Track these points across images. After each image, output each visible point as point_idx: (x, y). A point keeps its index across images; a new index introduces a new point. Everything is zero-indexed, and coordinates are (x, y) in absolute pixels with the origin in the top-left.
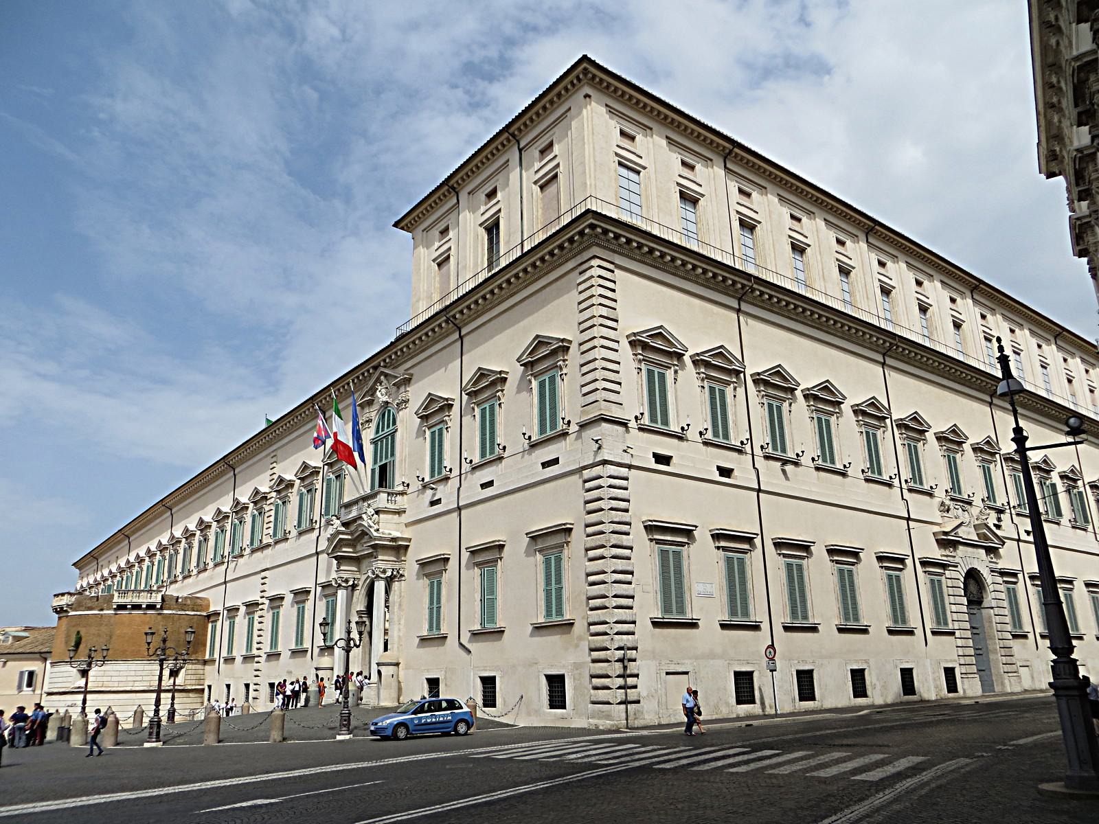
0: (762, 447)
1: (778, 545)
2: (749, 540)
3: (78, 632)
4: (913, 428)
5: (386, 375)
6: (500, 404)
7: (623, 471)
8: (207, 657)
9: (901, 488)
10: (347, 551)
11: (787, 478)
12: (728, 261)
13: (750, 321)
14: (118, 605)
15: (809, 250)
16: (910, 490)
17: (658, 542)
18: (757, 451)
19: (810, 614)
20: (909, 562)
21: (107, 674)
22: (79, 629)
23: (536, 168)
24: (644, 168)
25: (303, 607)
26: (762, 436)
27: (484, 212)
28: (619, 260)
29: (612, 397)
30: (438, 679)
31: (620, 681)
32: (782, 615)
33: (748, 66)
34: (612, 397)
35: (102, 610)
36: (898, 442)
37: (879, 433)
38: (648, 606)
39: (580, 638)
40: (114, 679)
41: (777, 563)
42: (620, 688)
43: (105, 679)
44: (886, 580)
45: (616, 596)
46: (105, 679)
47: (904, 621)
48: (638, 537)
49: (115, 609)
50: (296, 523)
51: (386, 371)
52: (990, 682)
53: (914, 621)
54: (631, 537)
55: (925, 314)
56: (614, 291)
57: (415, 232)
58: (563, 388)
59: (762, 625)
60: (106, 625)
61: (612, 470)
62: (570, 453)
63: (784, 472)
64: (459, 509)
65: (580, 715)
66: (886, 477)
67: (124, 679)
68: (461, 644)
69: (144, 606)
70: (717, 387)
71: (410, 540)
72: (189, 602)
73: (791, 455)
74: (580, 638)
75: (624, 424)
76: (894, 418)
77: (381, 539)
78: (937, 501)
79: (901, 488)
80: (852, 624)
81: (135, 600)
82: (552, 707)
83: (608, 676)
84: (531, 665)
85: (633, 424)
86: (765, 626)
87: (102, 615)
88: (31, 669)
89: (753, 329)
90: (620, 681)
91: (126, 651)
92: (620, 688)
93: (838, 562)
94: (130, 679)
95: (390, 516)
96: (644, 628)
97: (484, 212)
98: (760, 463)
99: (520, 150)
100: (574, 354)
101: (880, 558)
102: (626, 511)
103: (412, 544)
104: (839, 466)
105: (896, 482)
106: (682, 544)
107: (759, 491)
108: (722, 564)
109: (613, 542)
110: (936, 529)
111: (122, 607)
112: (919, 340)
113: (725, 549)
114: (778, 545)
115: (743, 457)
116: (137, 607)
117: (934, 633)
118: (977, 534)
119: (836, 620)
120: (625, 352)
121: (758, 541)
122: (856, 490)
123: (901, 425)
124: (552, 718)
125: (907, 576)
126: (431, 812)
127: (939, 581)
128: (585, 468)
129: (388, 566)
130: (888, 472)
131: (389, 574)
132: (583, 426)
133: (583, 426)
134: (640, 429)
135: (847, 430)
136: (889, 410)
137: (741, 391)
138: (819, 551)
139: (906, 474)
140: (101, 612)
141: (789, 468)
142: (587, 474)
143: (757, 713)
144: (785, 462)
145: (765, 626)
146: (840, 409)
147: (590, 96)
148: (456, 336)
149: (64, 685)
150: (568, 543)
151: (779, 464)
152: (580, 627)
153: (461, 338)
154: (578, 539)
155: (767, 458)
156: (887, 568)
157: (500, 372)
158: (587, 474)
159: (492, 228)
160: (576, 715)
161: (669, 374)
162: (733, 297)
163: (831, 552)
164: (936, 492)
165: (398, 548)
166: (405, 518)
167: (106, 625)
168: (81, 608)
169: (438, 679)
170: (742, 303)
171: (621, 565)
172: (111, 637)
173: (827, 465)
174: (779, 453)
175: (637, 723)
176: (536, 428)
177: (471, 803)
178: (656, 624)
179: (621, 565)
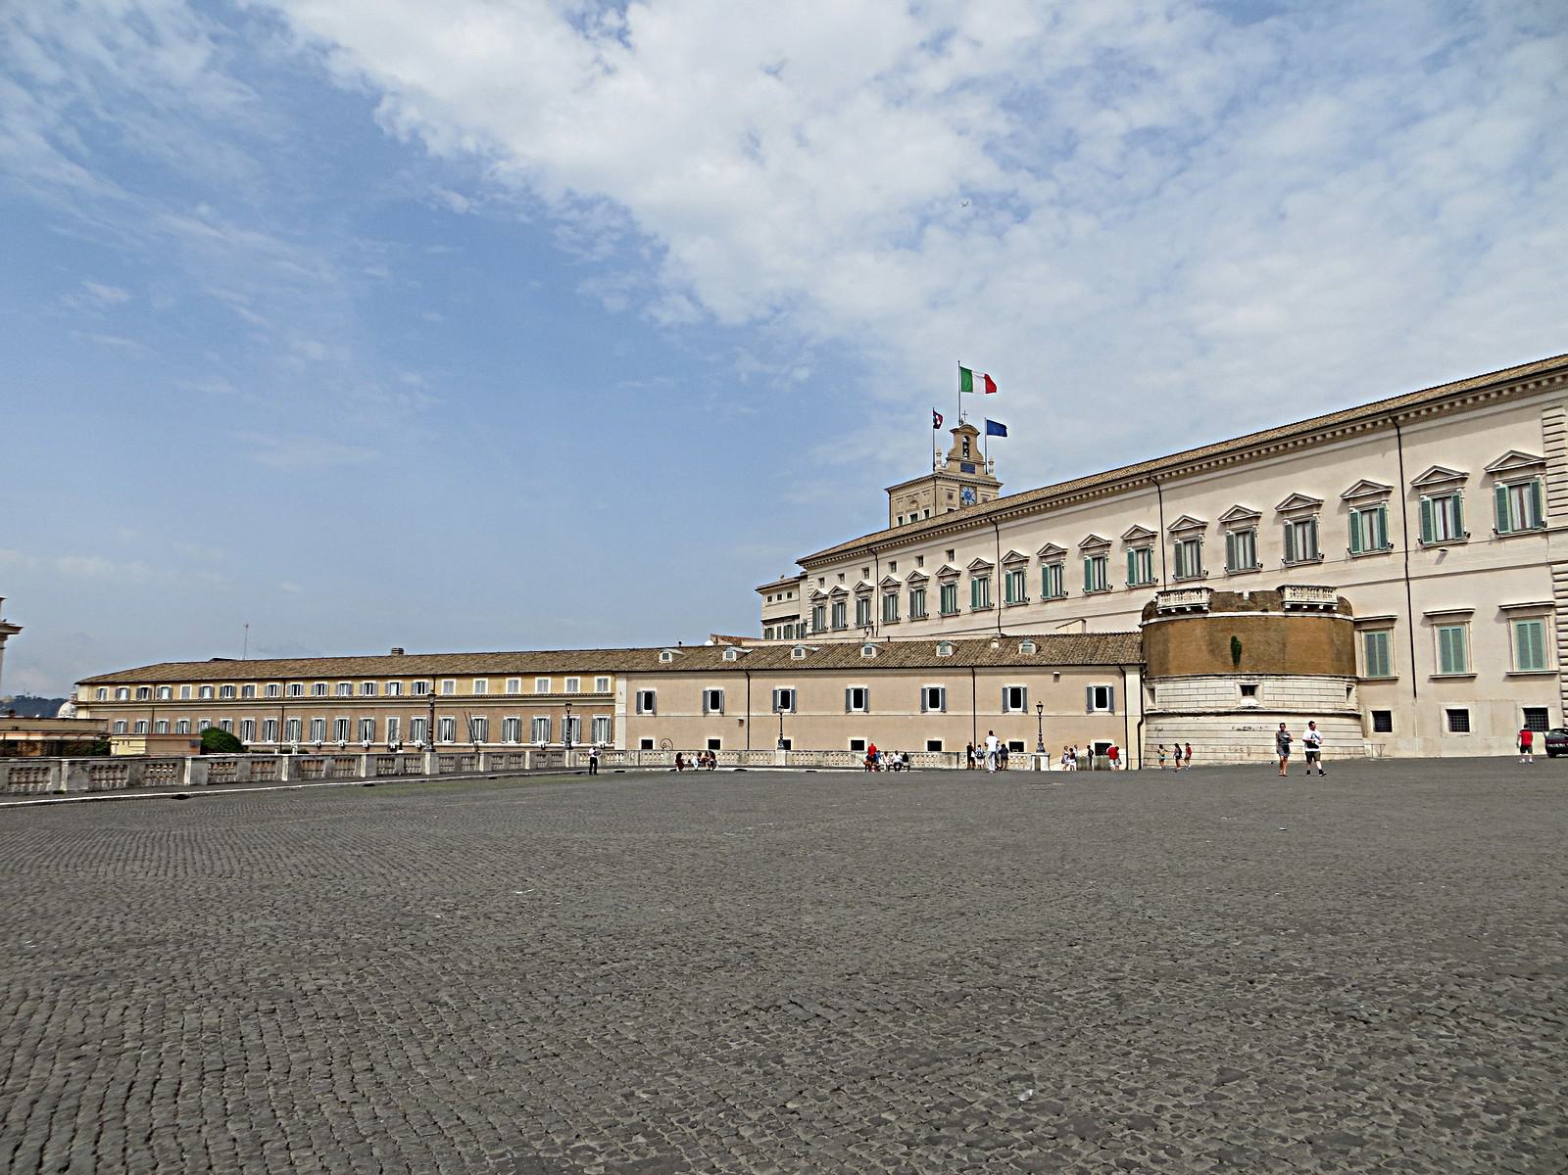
3: (1234, 639)
8: (1362, 672)
14: (1292, 605)
21: (1287, 691)
22: (1235, 635)
33: (962, 187)
35: (1266, 610)
40: (1297, 698)
43: (1286, 698)
46: (1286, 698)
52: (55, 745)
60: (1275, 630)
67: (1309, 698)
69: (1321, 607)
81: (1312, 599)
87: (1267, 617)
88: (1101, 684)
91: (1304, 664)
94: (1315, 698)
111: (1296, 607)
116: (1313, 608)
140: (1265, 614)
143: (1256, 759)
149: (1219, 704)
150: (1392, 628)
153: (1399, 436)
167: (1275, 630)
168: (1229, 608)
169: (1390, 712)
172: (1284, 645)
178: (1435, 679)
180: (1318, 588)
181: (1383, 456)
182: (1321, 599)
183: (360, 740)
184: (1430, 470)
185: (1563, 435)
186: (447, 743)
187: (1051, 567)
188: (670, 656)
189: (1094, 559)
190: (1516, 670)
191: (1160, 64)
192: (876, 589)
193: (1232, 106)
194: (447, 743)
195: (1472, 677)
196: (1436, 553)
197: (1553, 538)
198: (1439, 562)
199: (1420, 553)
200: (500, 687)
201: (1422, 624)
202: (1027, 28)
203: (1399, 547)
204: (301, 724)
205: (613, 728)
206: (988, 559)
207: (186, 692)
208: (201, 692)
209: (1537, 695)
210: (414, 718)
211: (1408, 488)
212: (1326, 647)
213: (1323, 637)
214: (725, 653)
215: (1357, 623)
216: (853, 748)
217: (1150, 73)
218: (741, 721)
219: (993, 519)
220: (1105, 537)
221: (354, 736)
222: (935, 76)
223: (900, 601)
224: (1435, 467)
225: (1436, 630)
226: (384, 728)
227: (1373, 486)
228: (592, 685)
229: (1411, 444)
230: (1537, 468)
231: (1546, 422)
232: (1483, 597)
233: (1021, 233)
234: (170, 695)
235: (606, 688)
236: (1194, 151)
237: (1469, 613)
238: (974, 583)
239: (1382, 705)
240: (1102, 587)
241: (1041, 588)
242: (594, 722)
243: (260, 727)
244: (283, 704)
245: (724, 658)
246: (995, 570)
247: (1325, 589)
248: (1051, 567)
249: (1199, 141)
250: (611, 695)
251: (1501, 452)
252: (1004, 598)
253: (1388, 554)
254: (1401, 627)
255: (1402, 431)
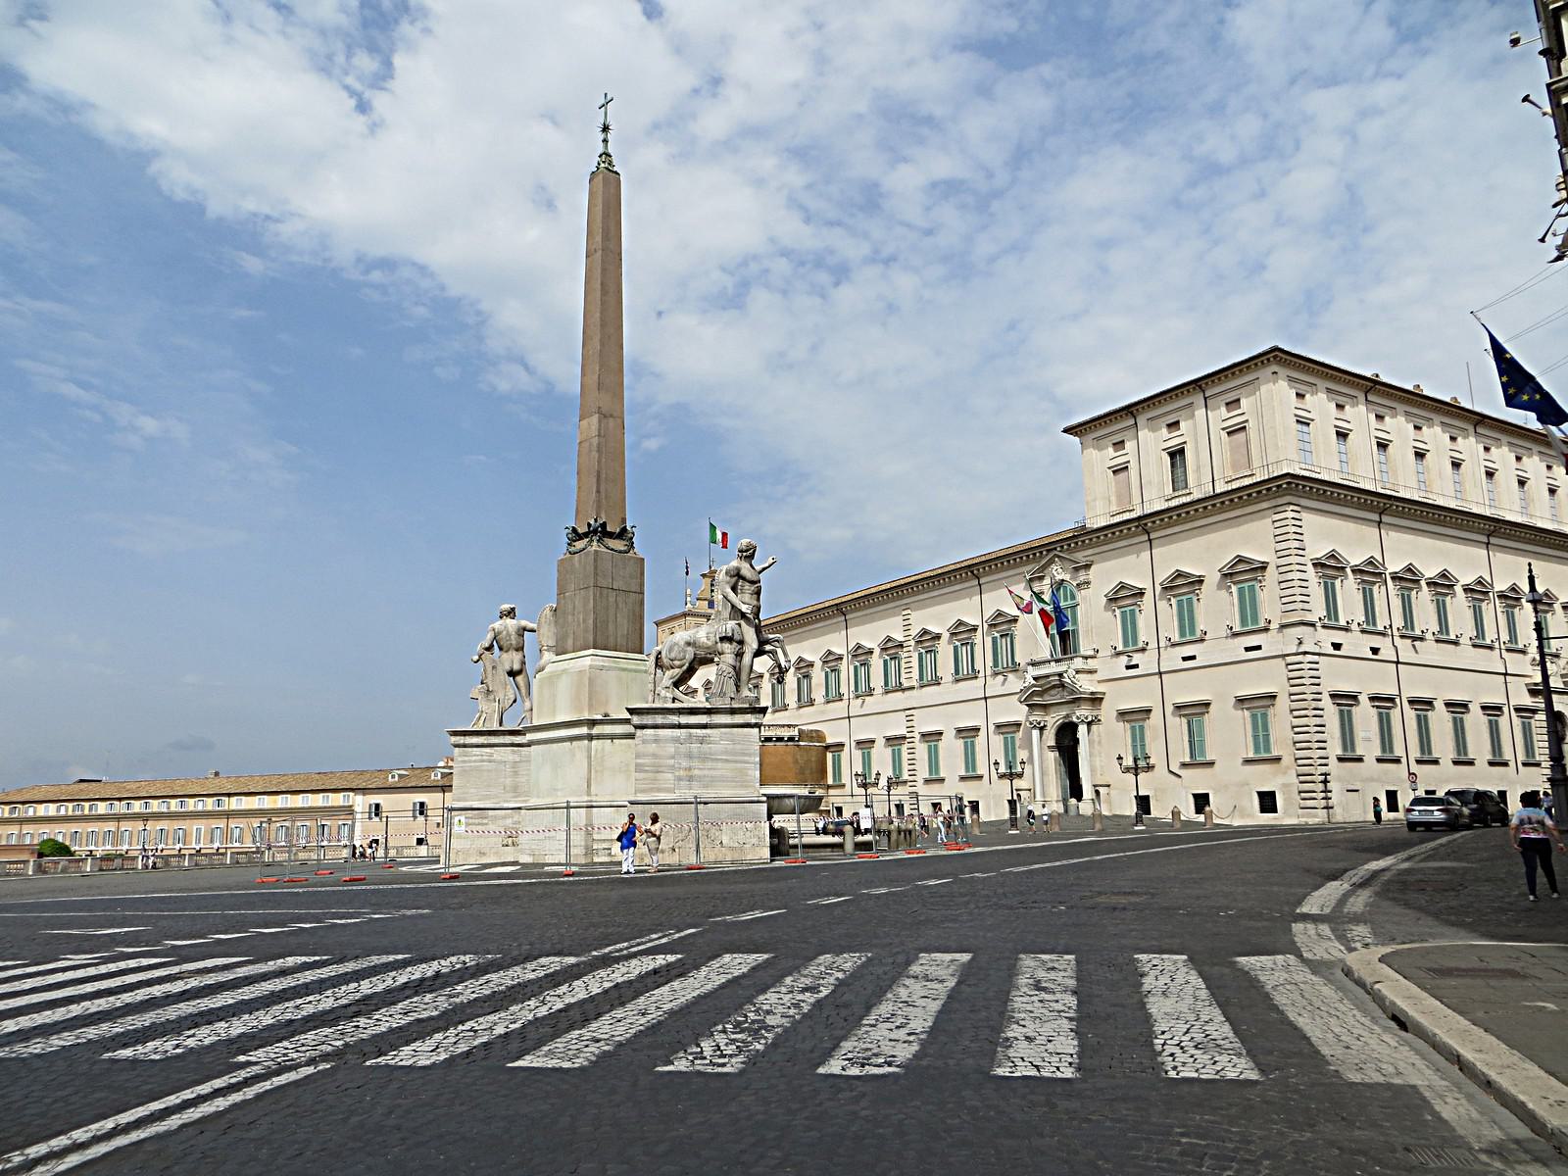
0: (1398, 629)
1: (1411, 702)
2: (1392, 700)
4: (1408, 579)
5: (1059, 557)
6: (1198, 600)
7: (1316, 658)
8: (830, 781)
9: (1500, 649)
10: (1037, 700)
11: (1417, 652)
12: (1372, 488)
13: (1392, 534)
15: (1428, 455)
16: (1508, 650)
17: (1338, 705)
18: (1395, 632)
19: (1433, 751)
20: (1506, 709)
23: (1220, 415)
24: (1313, 420)
25: (973, 743)
26: (1398, 622)
27: (1167, 439)
28: (1304, 502)
29: (1306, 606)
30: (1148, 796)
31: (1323, 795)
32: (1415, 753)
34: (1306, 606)
36: (1499, 610)
37: (1484, 605)
38: (1335, 749)
39: (1288, 768)
41: (1411, 714)
42: (1323, 799)
44: (1487, 724)
45: (1317, 742)
47: (1500, 755)
48: (1326, 702)
49: (762, 741)
50: (953, 671)
51: (1061, 554)
53: (1508, 755)
54: (1323, 702)
55: (1523, 487)
56: (1301, 527)
57: (1085, 438)
58: (1263, 597)
59: (1402, 760)
61: (1309, 658)
62: (1269, 643)
63: (1414, 646)
64: (1160, 674)
65: (1290, 816)
66: (1488, 642)
68: (1171, 772)
70: (1368, 587)
71: (1104, 694)
72: (814, 735)
73: (1418, 632)
74: (1288, 768)
75: (1313, 625)
76: (1496, 590)
77: (1085, 693)
78: (1529, 657)
79: (1500, 649)
80: (1463, 758)
82: (1262, 811)
83: (1314, 792)
84: (1243, 785)
85: (1318, 624)
86: (1404, 760)
89: (1392, 537)
90: (1323, 795)
92: (1323, 799)
93: (1453, 712)
95: (1085, 675)
96: (1333, 761)
97: (1167, 439)
98: (1397, 640)
99: (1205, 399)
100: (1271, 570)
101: (1484, 708)
102: (1318, 685)
103: (1106, 697)
104: (1453, 637)
105: (1497, 645)
106: (1351, 705)
107: (1398, 663)
108: (1375, 719)
109: (1314, 706)
110: (1528, 680)
112: (1519, 519)
113: (1378, 707)
114: (1411, 702)
115: (1387, 638)
116: (780, 739)
117: (1524, 764)
118: (1564, 682)
119: (1452, 755)
120: (1311, 572)
121: (1398, 700)
122: (1467, 656)
123: (1502, 596)
124: (1267, 819)
125: (1503, 721)
126: (236, 1097)
127: (1529, 723)
128: (1288, 655)
129: (1086, 713)
130: (1490, 636)
131: (1090, 719)
132: (1283, 627)
133: (1283, 627)
134: (1323, 627)
135: (1459, 605)
136: (1492, 585)
137: (1383, 588)
138: (1439, 705)
139: (1505, 637)
141: (1417, 643)
142: (1290, 659)
144: (1415, 639)
145: (1404, 760)
146: (1454, 590)
147: (1276, 373)
148: (843, 618)
150: (1273, 705)
151: (1409, 641)
152: (1287, 760)
153: (846, 620)
154: (1283, 703)
155: (1402, 637)
156: (1489, 715)
157: (1200, 576)
158: (1290, 659)
159: (1177, 455)
160: (1286, 815)
161: (1338, 583)
162: (1375, 512)
163: (1448, 705)
164: (1529, 650)
165: (1096, 700)
166: (1096, 677)
169: (1148, 796)
170: (1383, 517)
171: (1318, 721)
173: (1444, 639)
174: (1410, 632)
175: (1333, 821)
176: (1238, 622)
177: (207, 1109)
179: (1318, 721)
180: (783, 726)
181: (1138, 556)
182: (786, 733)
183: (174, 844)
184: (1173, 574)
185: (910, 627)
186: (237, 845)
187: (1001, 636)
188: (397, 776)
189: (861, 665)
190: (1251, 755)
191: (939, 111)
192: (845, 658)
193: (1020, 156)
194: (237, 845)
195: (1211, 764)
196: (1000, 678)
197: (907, 693)
198: (1003, 683)
199: (1229, 640)
200: (275, 802)
201: (1173, 714)
202: (796, 71)
203: (982, 674)
204: (131, 833)
205: (353, 831)
206: (972, 620)
207: (47, 809)
208: (58, 810)
209: (1266, 779)
210: (214, 826)
211: (1158, 588)
212: (792, 765)
213: (790, 759)
214: (433, 774)
215: (827, 747)
216: (418, 844)
217: (929, 121)
218: (438, 824)
219: (975, 572)
220: (935, 630)
221: (170, 841)
222: (714, 122)
223: (814, 681)
224: (1239, 556)
225: (1128, 725)
226: (192, 834)
227: (1187, 575)
228: (337, 800)
229: (1160, 546)
230: (1259, 571)
231: (1277, 524)
232: (945, 722)
233: (845, 295)
234: (35, 812)
235: (348, 802)
236: (995, 205)
237: (1207, 705)
238: (799, 679)
239: (1263, 786)
240: (1010, 665)
241: (824, 690)
242: (339, 827)
243: (102, 834)
244: (119, 818)
245: (433, 778)
246: (845, 660)
247: (789, 726)
248: (962, 644)
249: (997, 194)
250: (351, 806)
251: (1230, 557)
252: (852, 688)
253: (842, 700)
254: (1156, 717)
255: (1152, 536)
